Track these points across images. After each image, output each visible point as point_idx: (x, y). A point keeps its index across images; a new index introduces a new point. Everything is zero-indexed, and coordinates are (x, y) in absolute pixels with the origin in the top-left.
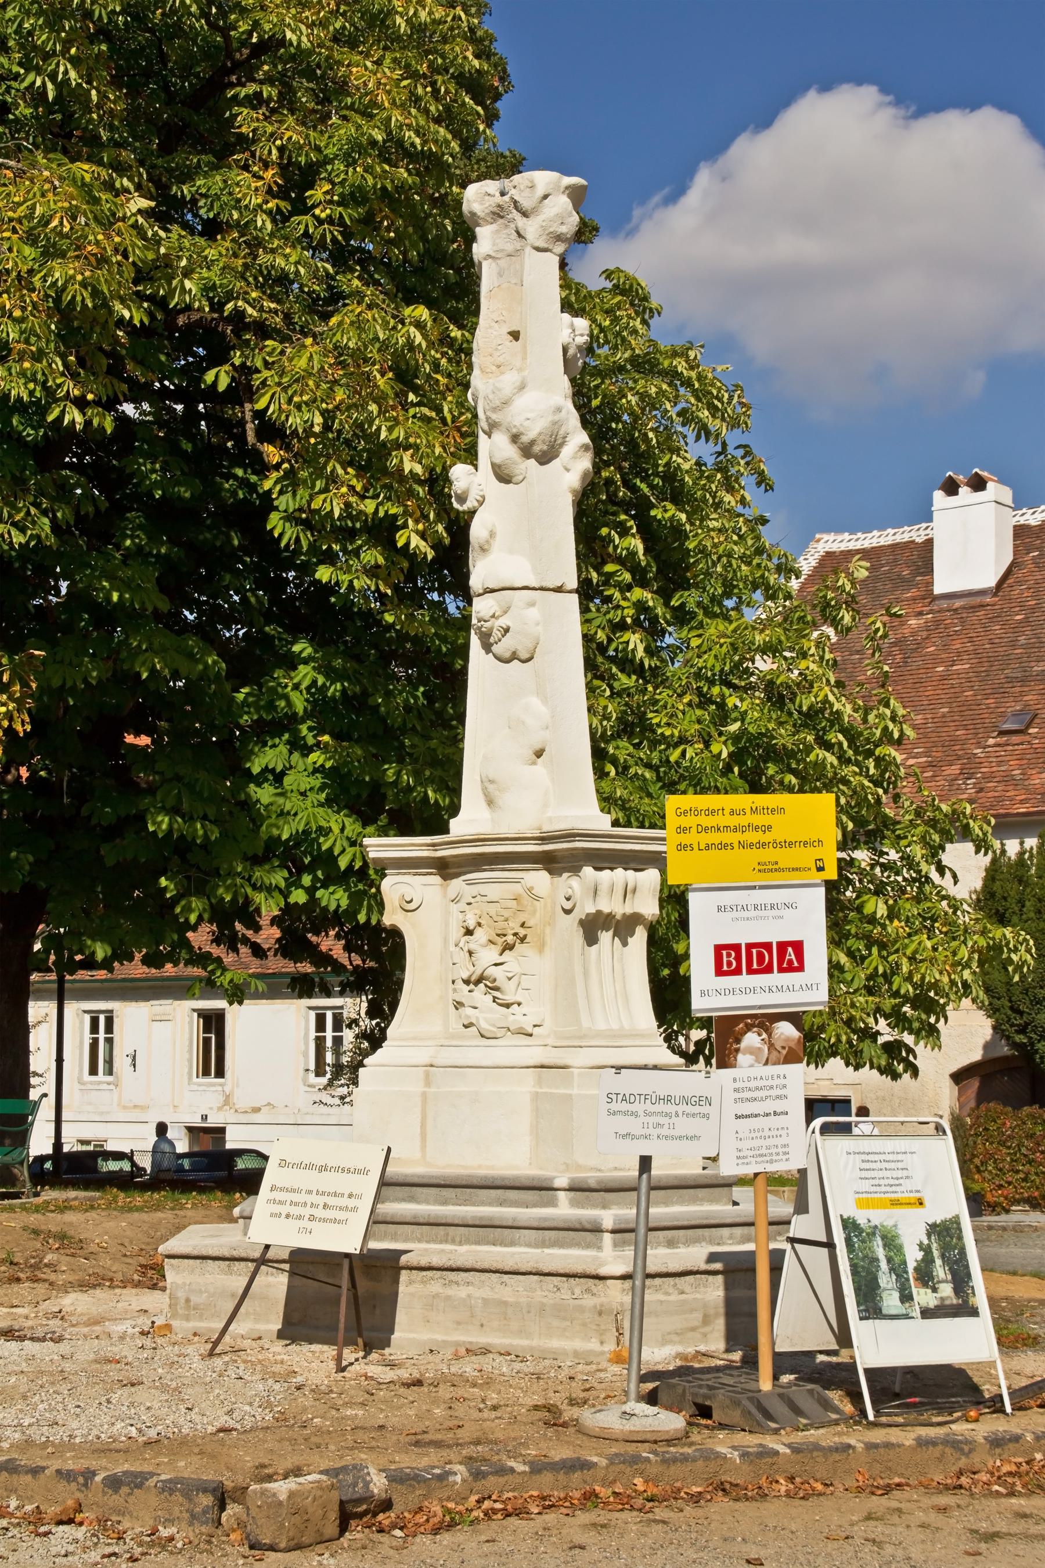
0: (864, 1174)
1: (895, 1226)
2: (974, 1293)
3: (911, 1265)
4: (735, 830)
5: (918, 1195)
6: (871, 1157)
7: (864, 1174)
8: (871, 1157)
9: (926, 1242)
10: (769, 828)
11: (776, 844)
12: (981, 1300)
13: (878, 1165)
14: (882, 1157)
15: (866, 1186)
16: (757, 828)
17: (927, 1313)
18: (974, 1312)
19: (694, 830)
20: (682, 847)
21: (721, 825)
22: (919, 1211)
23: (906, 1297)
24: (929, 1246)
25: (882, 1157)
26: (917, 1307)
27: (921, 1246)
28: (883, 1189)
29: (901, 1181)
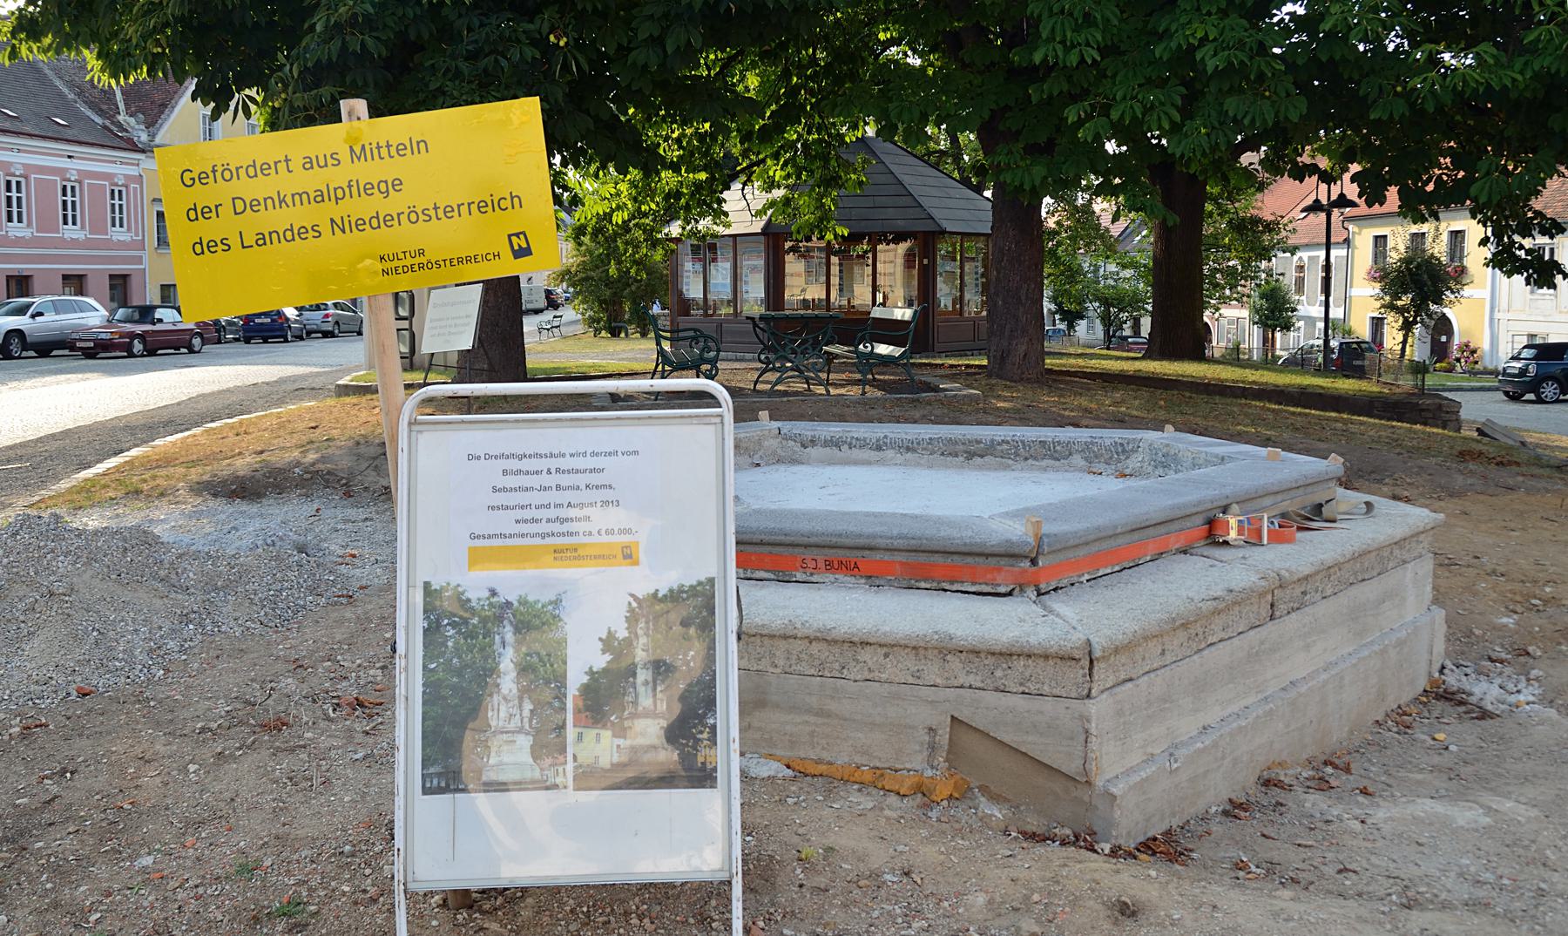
0: (501, 499)
1: (556, 603)
2: (713, 741)
3: (576, 679)
4: (320, 197)
5: (626, 539)
6: (526, 465)
7: (501, 499)
8: (526, 465)
9: (622, 633)
10: (397, 184)
11: (414, 216)
12: (728, 756)
13: (546, 480)
14: (553, 464)
15: (505, 522)
16: (368, 189)
17: (587, 778)
18: (703, 777)
19: (226, 211)
20: (203, 247)
21: (287, 191)
22: (625, 571)
23: (549, 742)
24: (629, 643)
25: (553, 464)
26: (570, 766)
27: (608, 643)
28: (544, 527)
29: (586, 511)
